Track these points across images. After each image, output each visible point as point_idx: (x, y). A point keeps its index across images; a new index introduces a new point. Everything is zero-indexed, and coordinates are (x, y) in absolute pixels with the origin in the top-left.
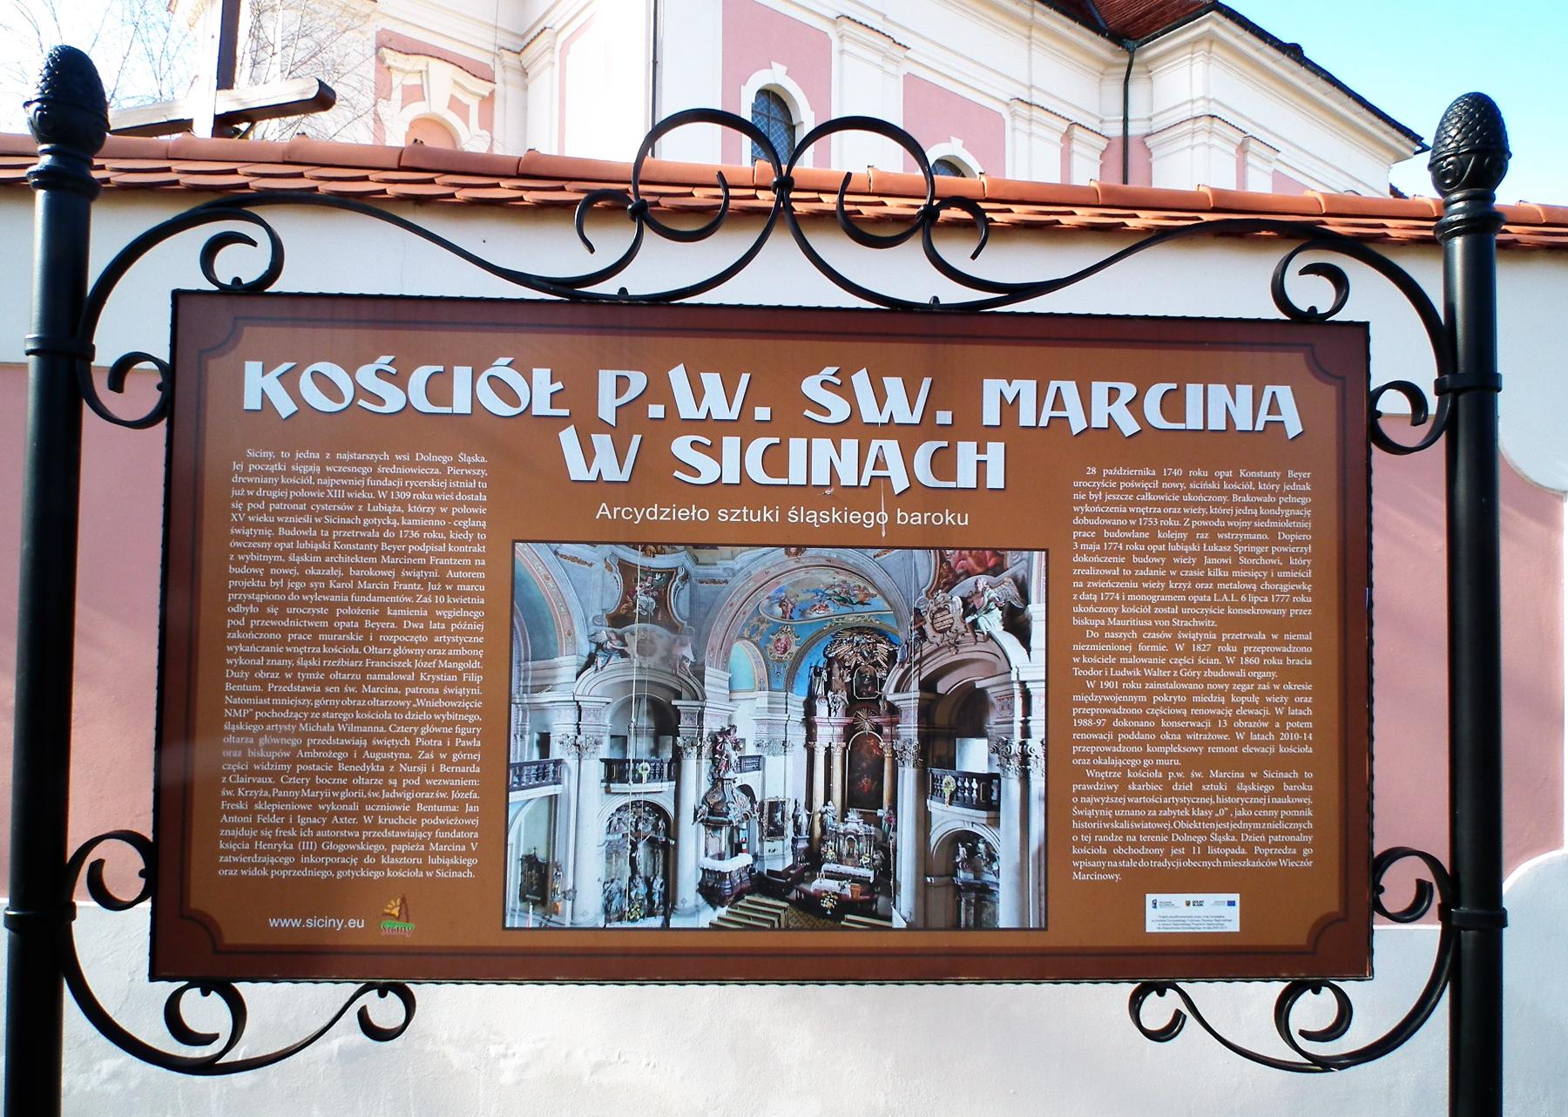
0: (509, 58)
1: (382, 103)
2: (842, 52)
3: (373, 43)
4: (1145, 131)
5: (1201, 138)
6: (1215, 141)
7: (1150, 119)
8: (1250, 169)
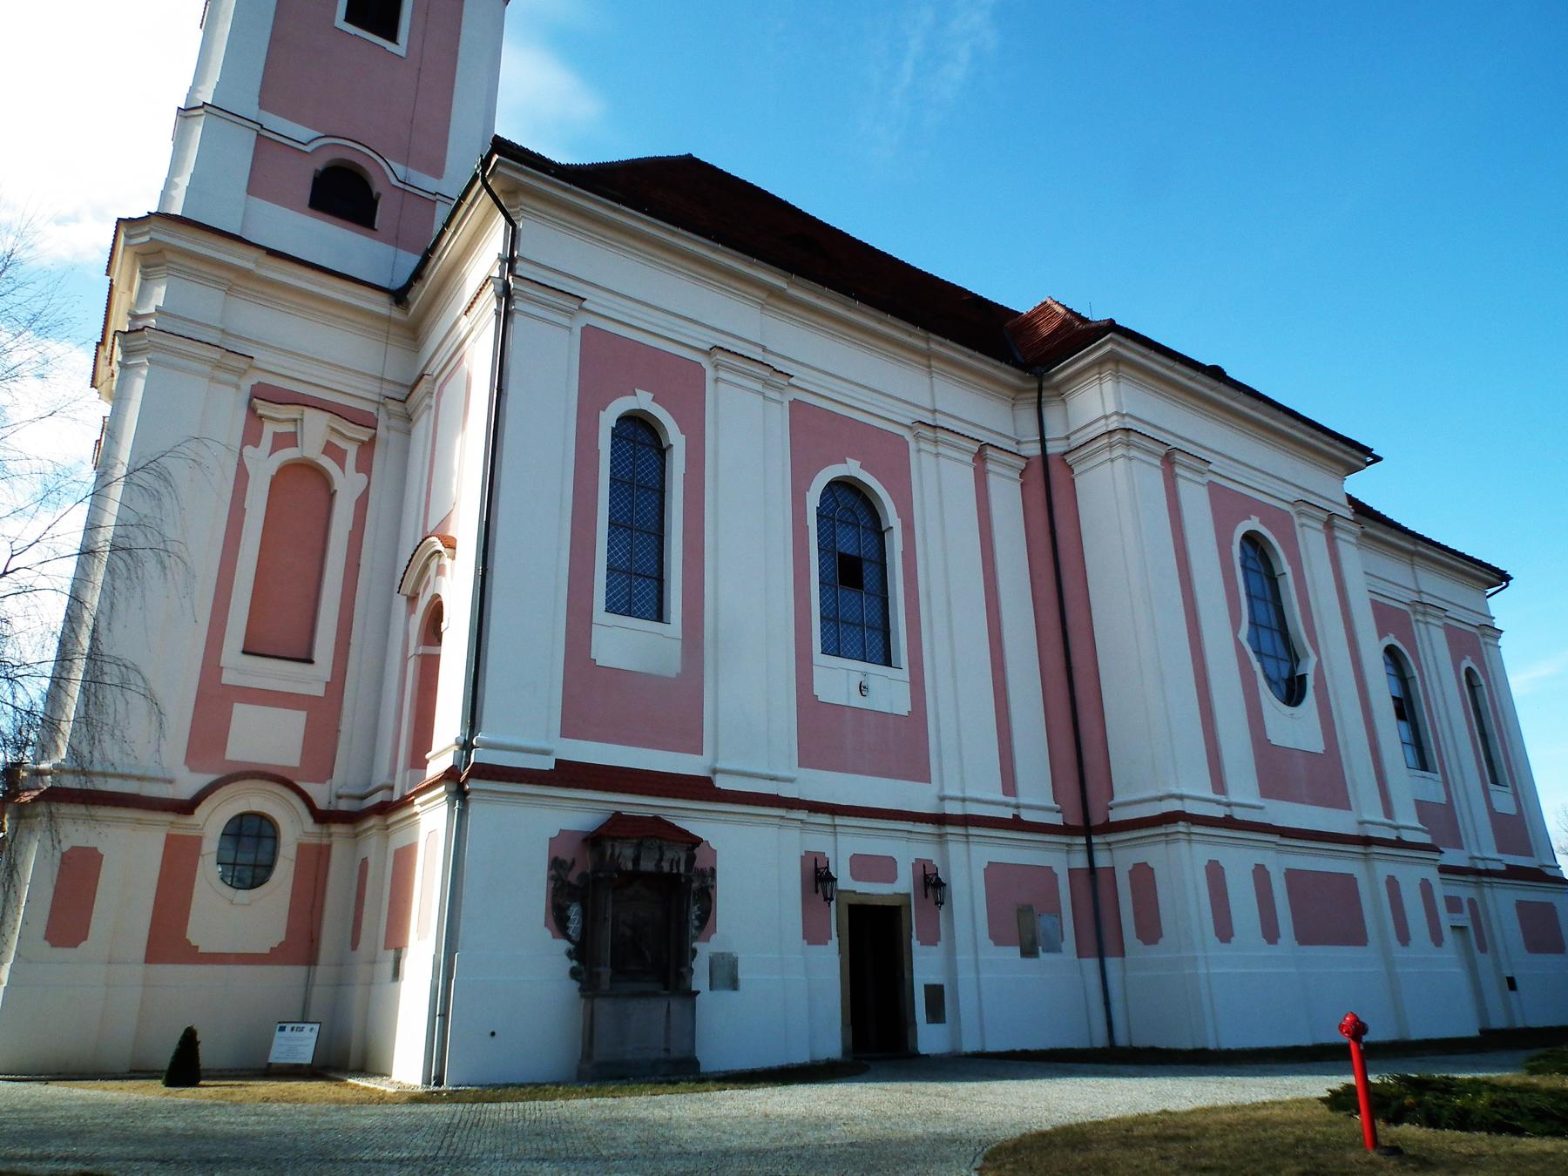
0: (394, 407)
1: (249, 450)
2: (717, 380)
3: (247, 397)
4: (1062, 450)
5: (1119, 451)
6: (1133, 453)
7: (1068, 438)
8: (1180, 481)
